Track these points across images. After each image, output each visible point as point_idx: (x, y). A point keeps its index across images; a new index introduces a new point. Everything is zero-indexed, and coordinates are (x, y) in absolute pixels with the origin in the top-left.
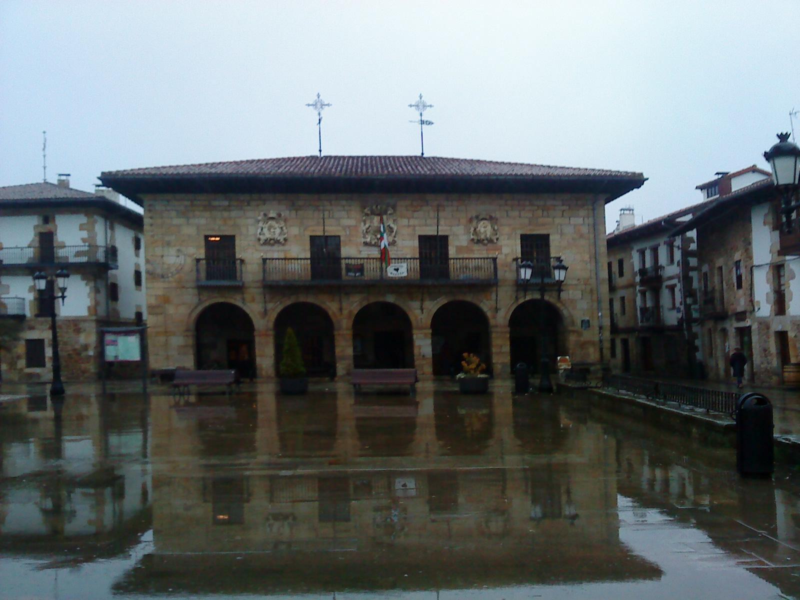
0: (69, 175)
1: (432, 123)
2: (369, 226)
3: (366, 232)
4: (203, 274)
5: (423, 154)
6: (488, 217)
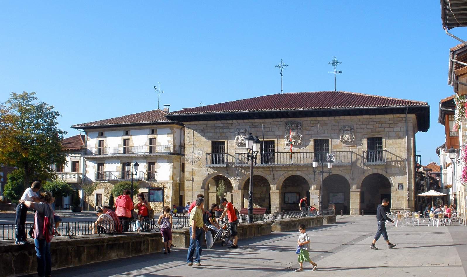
0: (169, 105)
4: (210, 161)
5: (336, 90)
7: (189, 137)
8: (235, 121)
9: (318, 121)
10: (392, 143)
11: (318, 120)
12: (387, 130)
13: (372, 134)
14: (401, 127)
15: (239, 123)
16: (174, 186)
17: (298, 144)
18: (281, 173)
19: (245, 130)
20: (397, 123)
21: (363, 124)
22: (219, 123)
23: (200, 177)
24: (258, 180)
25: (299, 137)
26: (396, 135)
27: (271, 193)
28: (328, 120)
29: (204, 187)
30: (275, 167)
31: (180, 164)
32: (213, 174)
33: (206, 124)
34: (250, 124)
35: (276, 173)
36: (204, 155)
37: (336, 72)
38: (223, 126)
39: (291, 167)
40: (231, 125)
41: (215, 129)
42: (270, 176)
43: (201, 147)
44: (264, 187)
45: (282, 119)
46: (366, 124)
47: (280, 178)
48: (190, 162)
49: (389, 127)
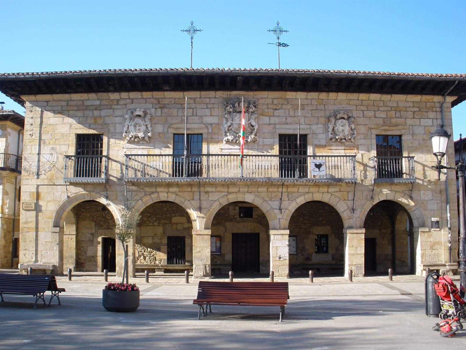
0: (3, 103)
1: (288, 46)
2: (232, 124)
3: (228, 130)
4: (71, 172)
6: (346, 117)
7: (32, 125)
8: (124, 95)
9: (287, 99)
10: (420, 145)
11: (287, 97)
12: (409, 122)
13: (386, 128)
14: (433, 119)
15: (132, 99)
16: (4, 222)
17: (249, 140)
18: (214, 197)
19: (144, 112)
20: (427, 110)
21: (367, 110)
22: (92, 99)
23: (50, 203)
24: (149, 215)
25: (251, 127)
26: (425, 132)
27: (194, 236)
28: (306, 99)
29: (59, 223)
30: (205, 185)
31: (16, 188)
32: (76, 198)
33: (67, 101)
34: (153, 100)
35: (204, 197)
36: (61, 158)
37: (280, 45)
38: (100, 105)
39: (236, 184)
40: (115, 103)
41: (83, 110)
42: (192, 202)
43: (55, 144)
44: (159, 226)
45: (220, 94)
46: (373, 111)
47: (213, 208)
48: (33, 173)
49: (413, 118)
